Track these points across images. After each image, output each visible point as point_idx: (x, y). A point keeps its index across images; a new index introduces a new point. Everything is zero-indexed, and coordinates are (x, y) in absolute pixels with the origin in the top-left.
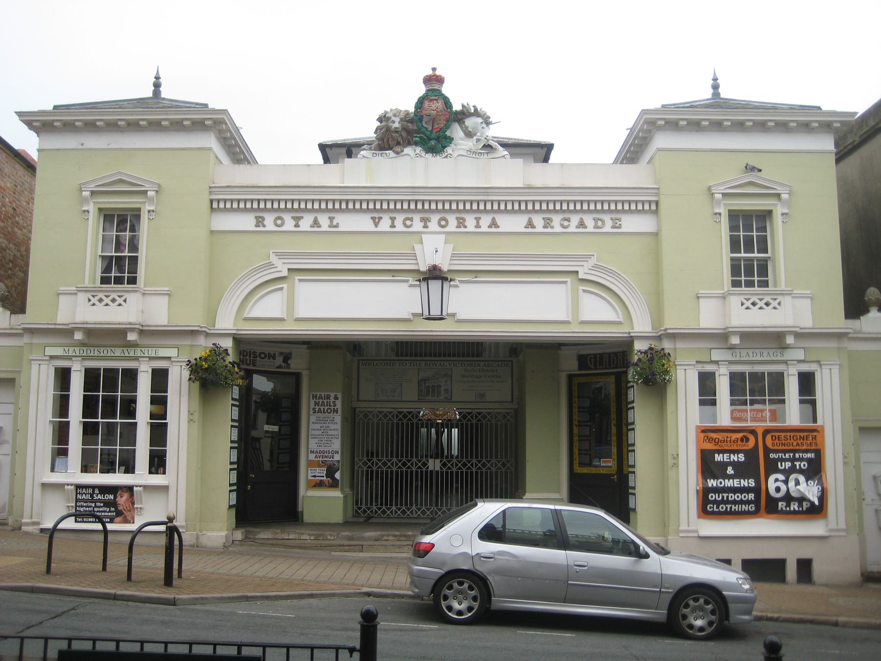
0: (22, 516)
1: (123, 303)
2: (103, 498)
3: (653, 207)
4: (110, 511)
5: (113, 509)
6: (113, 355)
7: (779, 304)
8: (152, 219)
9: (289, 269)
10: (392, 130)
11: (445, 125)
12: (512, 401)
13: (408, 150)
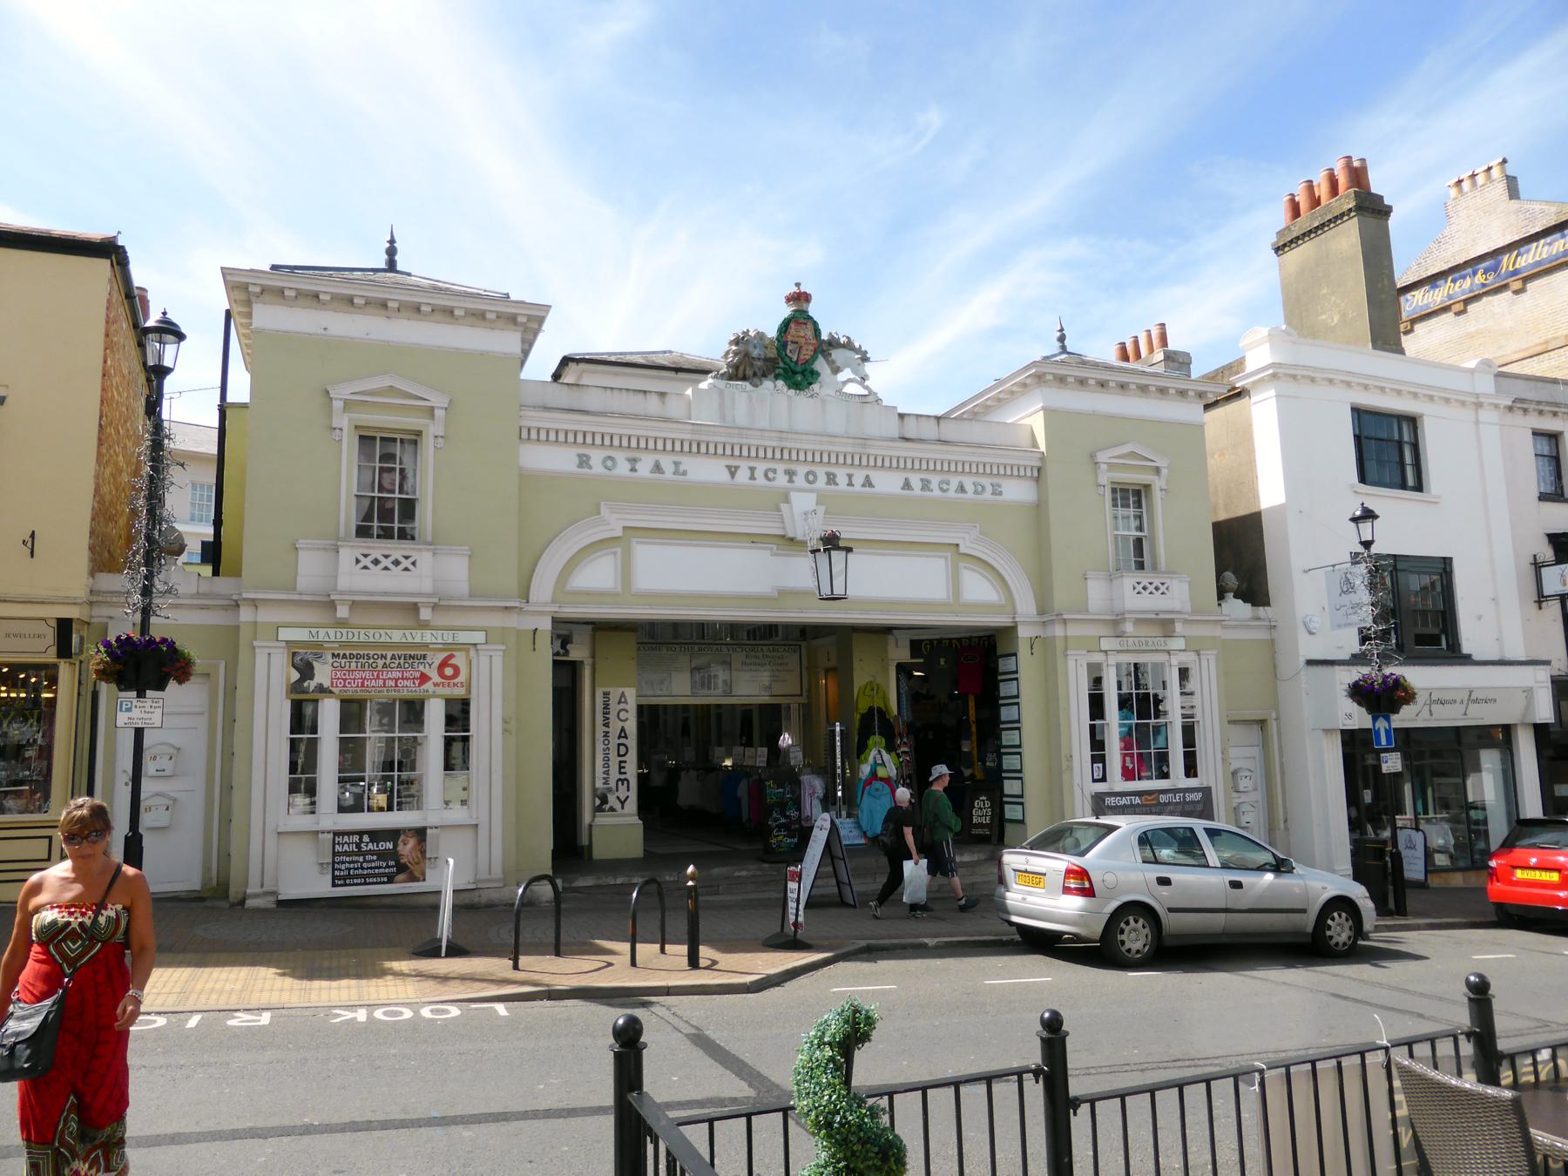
0: (246, 885)
1: (411, 567)
2: (376, 849)
3: (1036, 474)
4: (388, 866)
5: (392, 863)
6: (388, 640)
7: (1167, 589)
8: (441, 448)
9: (624, 528)
10: (754, 356)
11: (812, 357)
12: (801, 695)
13: (768, 384)
